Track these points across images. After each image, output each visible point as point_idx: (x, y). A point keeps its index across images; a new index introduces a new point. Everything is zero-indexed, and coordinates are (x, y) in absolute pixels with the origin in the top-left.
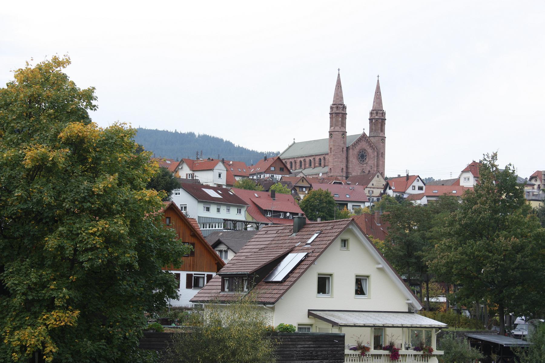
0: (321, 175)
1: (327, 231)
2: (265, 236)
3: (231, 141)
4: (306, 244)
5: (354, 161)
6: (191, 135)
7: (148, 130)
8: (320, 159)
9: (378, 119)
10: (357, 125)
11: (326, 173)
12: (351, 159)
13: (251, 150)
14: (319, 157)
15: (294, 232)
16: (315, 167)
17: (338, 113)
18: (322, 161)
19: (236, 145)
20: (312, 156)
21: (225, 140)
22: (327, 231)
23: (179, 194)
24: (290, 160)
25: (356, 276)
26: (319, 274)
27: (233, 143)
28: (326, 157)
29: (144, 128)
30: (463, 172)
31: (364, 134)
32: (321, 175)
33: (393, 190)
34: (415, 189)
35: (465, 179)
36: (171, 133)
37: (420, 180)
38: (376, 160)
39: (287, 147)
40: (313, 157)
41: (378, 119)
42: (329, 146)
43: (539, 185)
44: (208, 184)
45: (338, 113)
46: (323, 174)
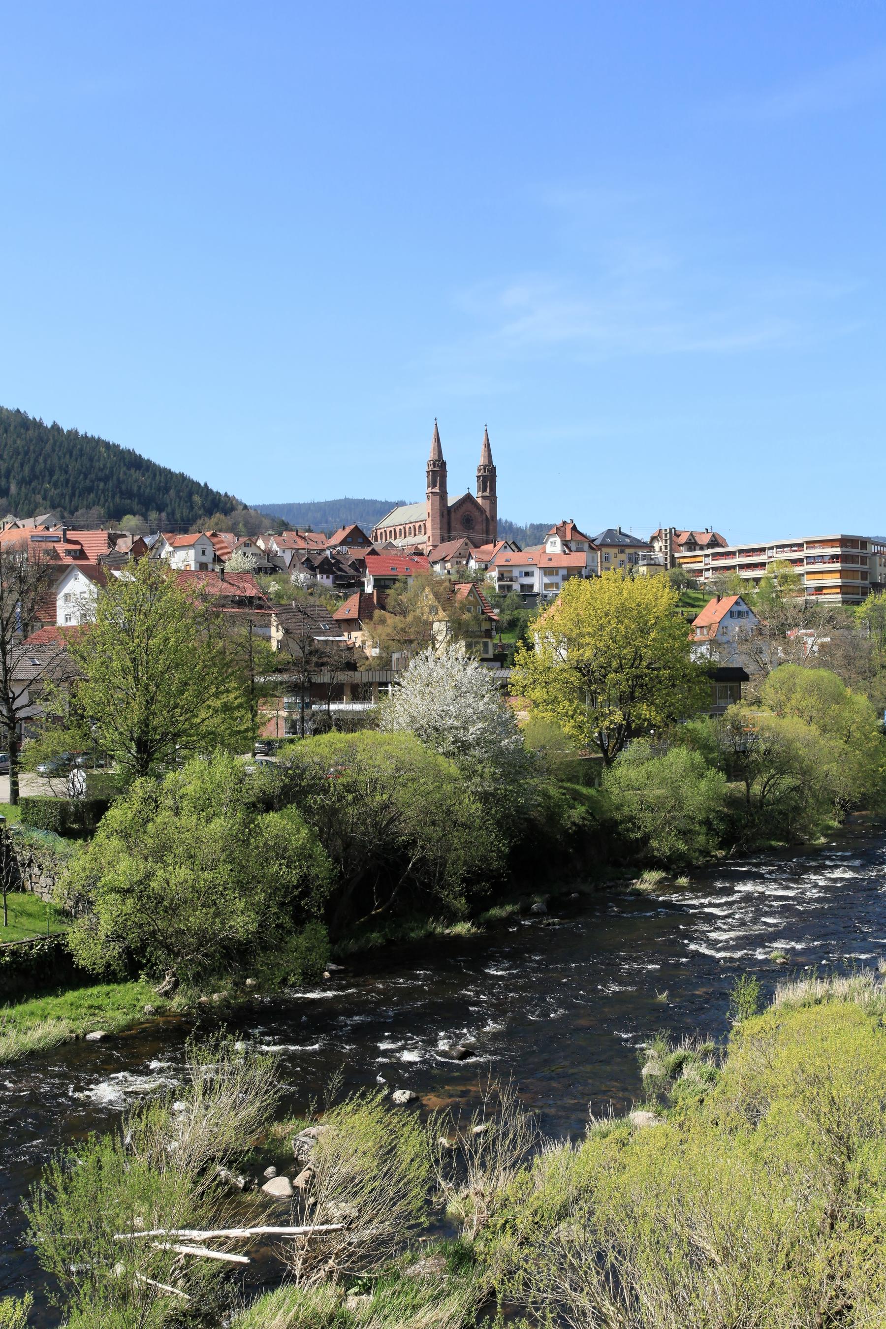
9: (488, 477)
12: (453, 524)
16: (415, 535)
17: (438, 472)
31: (468, 498)
36: (381, 503)
41: (488, 477)
45: (438, 472)
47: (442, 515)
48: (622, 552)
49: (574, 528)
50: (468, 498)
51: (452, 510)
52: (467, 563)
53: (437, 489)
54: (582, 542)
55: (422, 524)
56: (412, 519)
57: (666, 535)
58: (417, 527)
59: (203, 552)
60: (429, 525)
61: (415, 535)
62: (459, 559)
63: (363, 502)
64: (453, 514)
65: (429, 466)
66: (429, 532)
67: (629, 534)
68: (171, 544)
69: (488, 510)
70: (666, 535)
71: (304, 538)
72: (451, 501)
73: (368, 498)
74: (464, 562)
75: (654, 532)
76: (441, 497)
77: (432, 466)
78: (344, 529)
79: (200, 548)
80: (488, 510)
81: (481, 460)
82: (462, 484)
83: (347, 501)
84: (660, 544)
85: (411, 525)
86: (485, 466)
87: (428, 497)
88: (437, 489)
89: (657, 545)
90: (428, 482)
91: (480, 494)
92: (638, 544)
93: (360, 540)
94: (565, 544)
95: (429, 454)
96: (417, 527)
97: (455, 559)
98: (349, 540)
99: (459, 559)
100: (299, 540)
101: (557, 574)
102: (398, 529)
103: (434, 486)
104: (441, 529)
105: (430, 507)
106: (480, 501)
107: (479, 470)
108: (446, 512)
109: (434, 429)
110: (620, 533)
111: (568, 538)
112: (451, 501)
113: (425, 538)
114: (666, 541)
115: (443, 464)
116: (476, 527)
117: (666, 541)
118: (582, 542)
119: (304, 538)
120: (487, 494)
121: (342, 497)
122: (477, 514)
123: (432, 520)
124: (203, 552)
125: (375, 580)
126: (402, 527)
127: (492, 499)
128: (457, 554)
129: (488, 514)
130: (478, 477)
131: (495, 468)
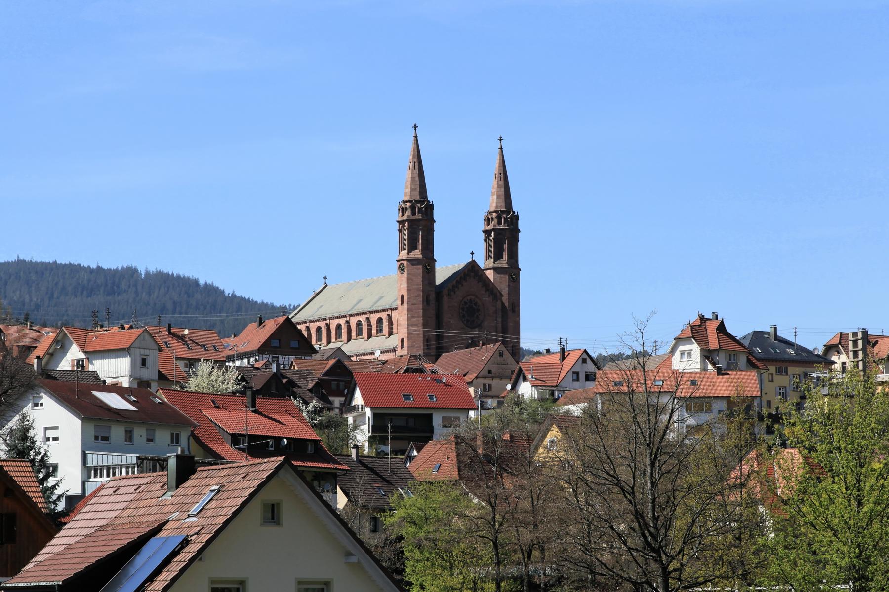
0: (378, 354)
1: (233, 486)
2: (112, 499)
3: (216, 284)
4: (189, 516)
5: (452, 321)
6: (131, 272)
7: (36, 264)
8: (319, 329)
9: (504, 232)
10: (459, 246)
11: (394, 350)
12: (446, 317)
13: (259, 301)
14: (377, 315)
15: (169, 490)
16: (370, 336)
17: (418, 222)
18: (386, 324)
19: (228, 291)
20: (365, 313)
21: (202, 282)
22: (233, 486)
23: (42, 404)
24: (318, 324)
25: (213, 582)
26: (213, 582)
27: (221, 287)
28: (394, 314)
29: (28, 259)
30: (679, 340)
31: (472, 267)
32: (378, 354)
33: (531, 382)
34: (578, 380)
35: (682, 354)
36: (89, 270)
37: (589, 360)
38: (500, 320)
39: (521, 265)
40: (365, 316)
41: (504, 232)
42: (399, 290)
43: (844, 363)
44: (120, 380)
45: (418, 222)
46: (382, 352)
47: (426, 301)
48: (782, 371)
49: (721, 328)
50: (472, 267)
51: (445, 292)
52: (514, 387)
53: (417, 254)
54: (736, 354)
55: (384, 315)
56: (364, 306)
57: (855, 343)
58: (374, 322)
59: (144, 362)
60: (401, 318)
61: (370, 336)
62: (488, 382)
63: (54, 268)
64: (445, 299)
65: (402, 210)
66: (402, 331)
67: (791, 339)
68: (82, 347)
69: (505, 292)
70: (855, 343)
71: (181, 338)
72: (442, 274)
73: (63, 260)
74: (509, 387)
75: (829, 337)
76: (425, 267)
77: (409, 212)
78: (261, 322)
79: (138, 353)
80: (505, 292)
81: (491, 202)
82: (459, 246)
83: (20, 263)
84: (843, 357)
85: (362, 319)
86: (500, 214)
87: (401, 269)
88: (417, 254)
89: (839, 359)
90: (401, 241)
91: (491, 263)
92: (807, 359)
93: (295, 344)
94: (708, 355)
95: (403, 191)
96: (374, 322)
97: (481, 381)
98: (275, 343)
99: (488, 382)
100: (174, 343)
101: (709, 410)
102: (334, 324)
103: (412, 247)
104: (425, 325)
105: (404, 285)
106: (490, 274)
107: (488, 220)
108: (433, 296)
109: (411, 146)
110: (777, 338)
111: (714, 344)
112: (442, 274)
113: (394, 341)
114: (856, 354)
115: (514, 220)
116: (486, 323)
117: (856, 354)
118: (736, 354)
119: (181, 338)
120: (504, 263)
121: (12, 258)
122: (487, 299)
123: (409, 310)
124: (144, 362)
125: (376, 416)
126: (342, 321)
127: (513, 273)
128: (485, 372)
129: (505, 299)
130: (487, 233)
131: (517, 217)
